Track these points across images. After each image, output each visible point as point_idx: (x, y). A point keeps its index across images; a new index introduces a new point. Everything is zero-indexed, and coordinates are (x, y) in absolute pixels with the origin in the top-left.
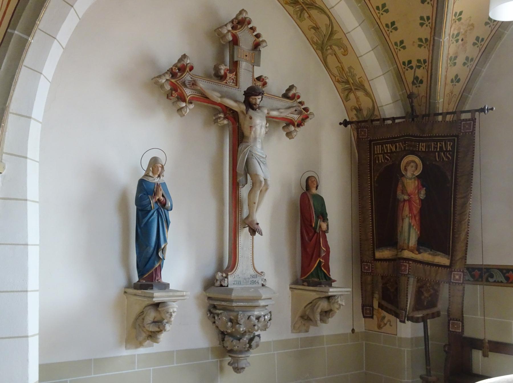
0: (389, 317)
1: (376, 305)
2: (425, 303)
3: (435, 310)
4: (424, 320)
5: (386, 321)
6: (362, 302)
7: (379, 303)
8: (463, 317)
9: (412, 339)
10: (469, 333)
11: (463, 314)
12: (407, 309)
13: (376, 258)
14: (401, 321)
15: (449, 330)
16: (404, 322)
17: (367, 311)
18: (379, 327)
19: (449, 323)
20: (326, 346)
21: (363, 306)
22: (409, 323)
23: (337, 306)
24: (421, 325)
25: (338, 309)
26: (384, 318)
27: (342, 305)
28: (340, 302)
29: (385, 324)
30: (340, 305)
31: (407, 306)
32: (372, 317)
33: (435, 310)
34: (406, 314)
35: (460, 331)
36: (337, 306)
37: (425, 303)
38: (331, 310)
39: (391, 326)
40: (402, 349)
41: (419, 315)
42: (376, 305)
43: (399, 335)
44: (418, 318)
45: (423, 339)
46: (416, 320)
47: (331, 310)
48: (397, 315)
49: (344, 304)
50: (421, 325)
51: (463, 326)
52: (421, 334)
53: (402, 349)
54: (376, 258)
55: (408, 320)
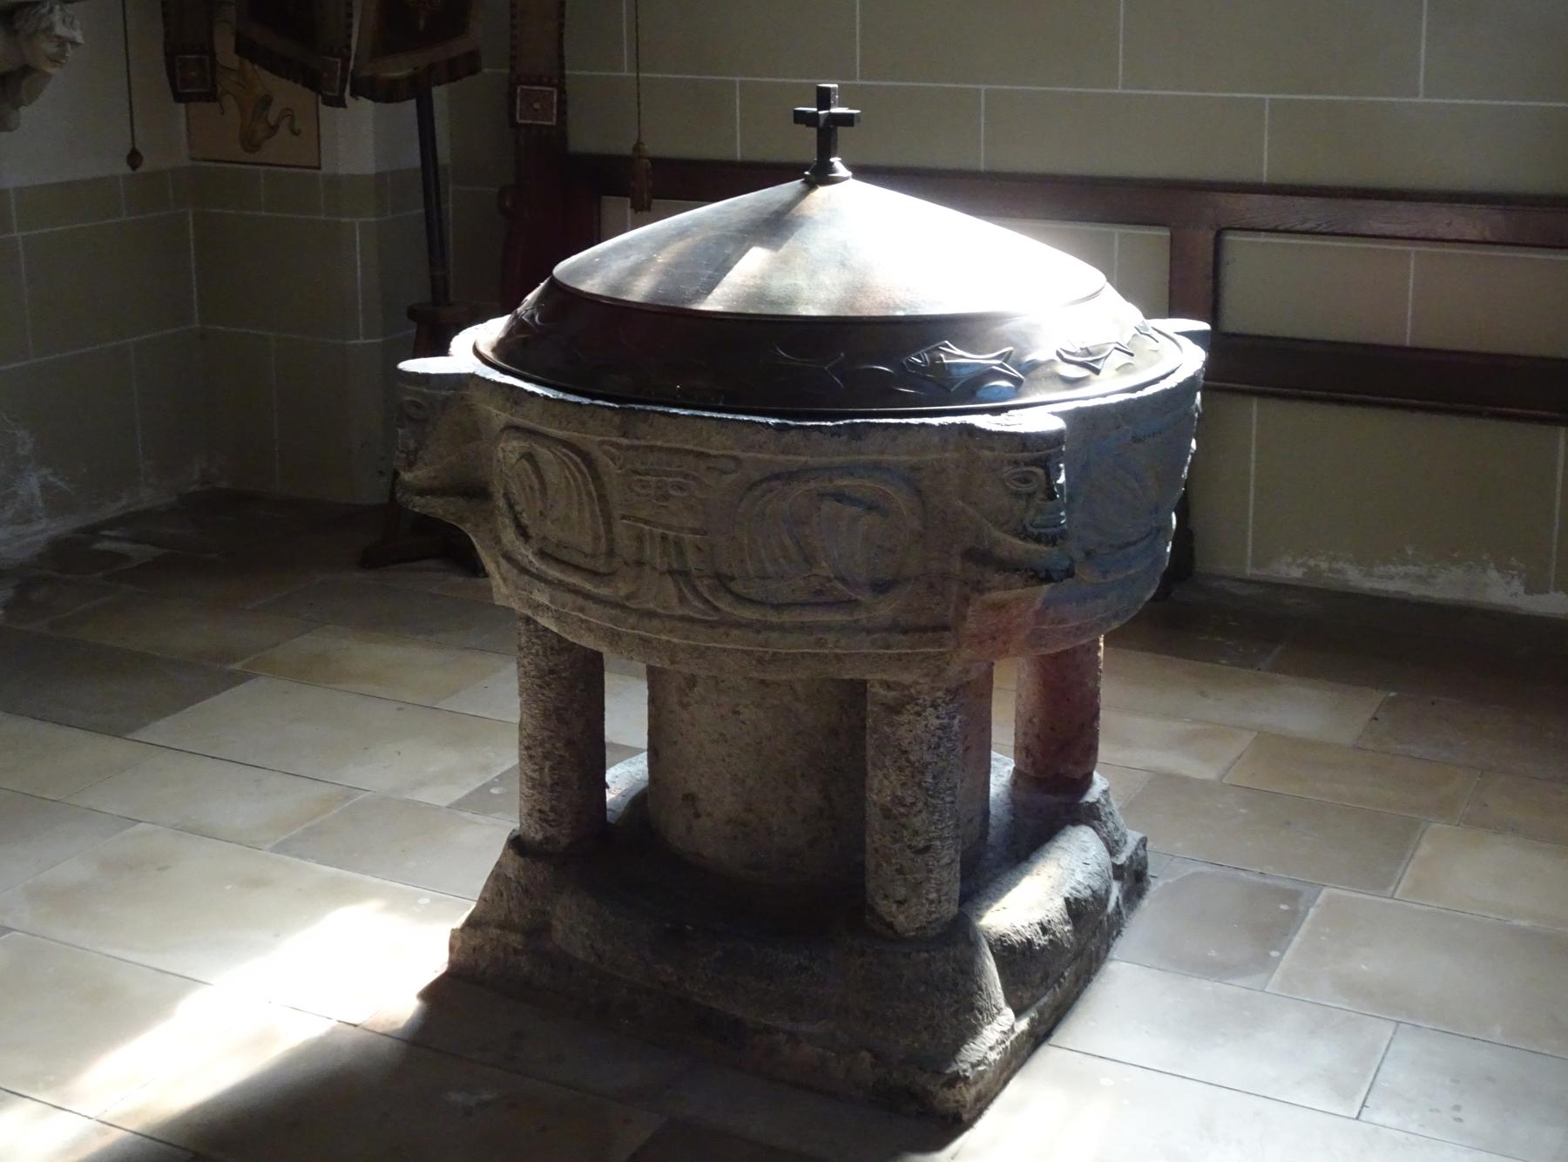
0: (287, 94)
1: (224, 44)
2: (422, 23)
3: (459, 47)
4: (417, 88)
5: (273, 115)
6: (167, 35)
7: (238, 36)
8: (563, 76)
9: (380, 177)
10: (586, 138)
11: (562, 67)
12: (349, 47)
13: (1230, 238)
14: (329, 102)
15: (514, 124)
16: (340, 103)
17: (190, 75)
18: (250, 143)
19: (512, 97)
20: (17, 235)
21: (172, 53)
22: (363, 109)
23: (51, 48)
24: (410, 107)
25: (54, 60)
26: (267, 101)
27: (74, 43)
28: (60, 30)
29: (273, 129)
30: (62, 42)
31: (350, 36)
32: (211, 96)
33: (459, 47)
34: (345, 68)
35: (554, 122)
36: (51, 48)
37: (422, 23)
38: (26, 70)
39: (295, 133)
40: (343, 220)
41: (398, 69)
42: (224, 44)
43: (326, 169)
44: (394, 82)
45: (420, 175)
46: (385, 93)
47: (26, 70)
48: (312, 81)
49: (79, 38)
50: (410, 107)
51: (562, 103)
52: (412, 158)
53: (343, 220)
54: (1230, 238)
55: (354, 94)
